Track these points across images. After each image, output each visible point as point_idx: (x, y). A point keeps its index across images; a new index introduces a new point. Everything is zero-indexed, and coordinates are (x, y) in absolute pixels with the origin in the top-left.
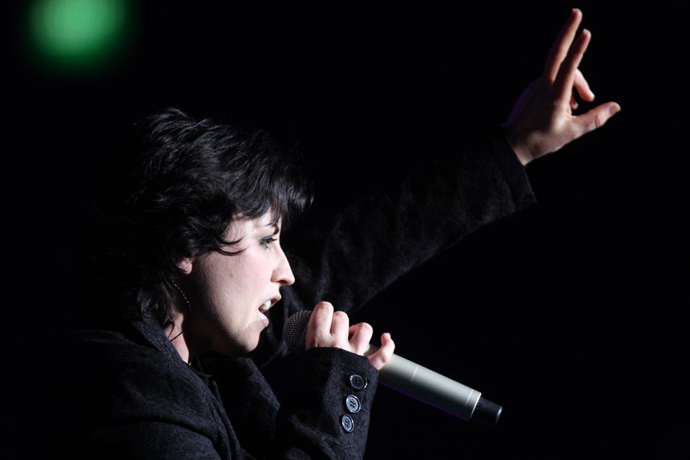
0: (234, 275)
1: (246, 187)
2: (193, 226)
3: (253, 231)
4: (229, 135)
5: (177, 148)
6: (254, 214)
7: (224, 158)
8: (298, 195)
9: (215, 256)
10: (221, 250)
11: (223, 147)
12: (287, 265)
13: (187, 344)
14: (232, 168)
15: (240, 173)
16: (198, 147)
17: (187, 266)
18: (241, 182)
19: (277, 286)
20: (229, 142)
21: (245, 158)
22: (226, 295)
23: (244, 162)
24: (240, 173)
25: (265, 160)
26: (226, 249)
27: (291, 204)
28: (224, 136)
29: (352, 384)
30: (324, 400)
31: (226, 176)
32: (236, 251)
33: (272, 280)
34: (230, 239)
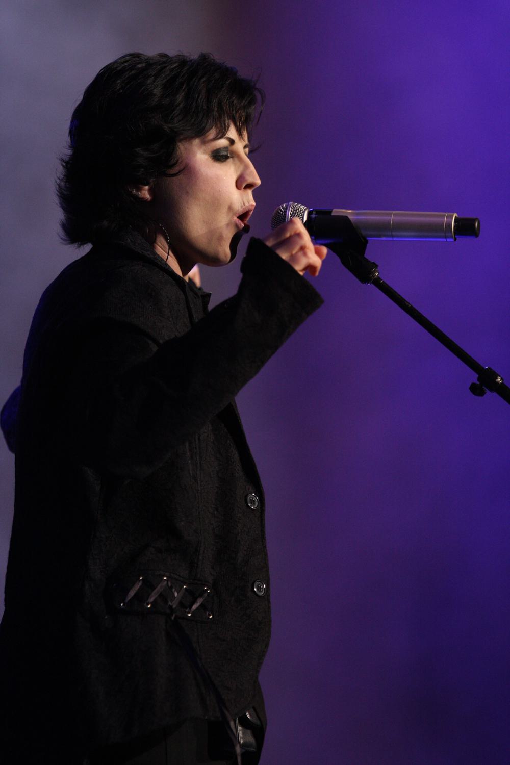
2: (362, 238)
6: (200, 133)
12: (252, 168)
17: (145, 193)
19: (250, 192)
22: (187, 210)
33: (238, 185)
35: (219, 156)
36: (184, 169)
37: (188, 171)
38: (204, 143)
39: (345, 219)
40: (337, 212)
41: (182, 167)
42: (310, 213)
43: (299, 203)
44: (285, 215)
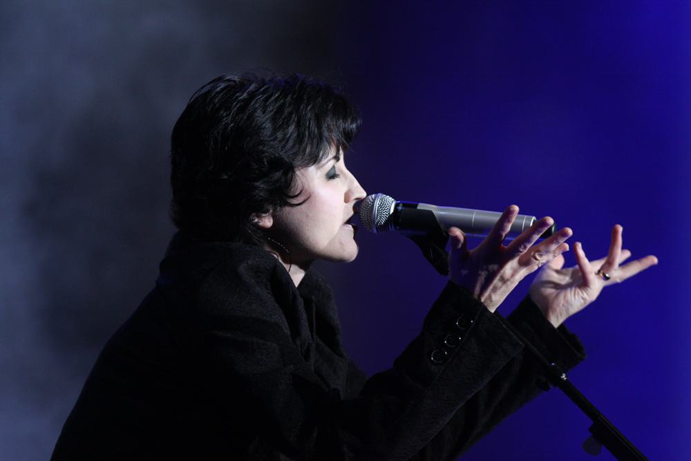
0: (310, 215)
1: (300, 139)
3: (317, 173)
4: (276, 93)
5: (232, 122)
6: (315, 159)
7: (274, 119)
8: (349, 121)
9: (287, 209)
10: (289, 203)
11: (271, 108)
12: (356, 183)
13: (363, 188)
14: (287, 123)
15: (292, 128)
16: (251, 116)
18: (295, 135)
20: (276, 100)
21: (290, 114)
23: (291, 118)
24: (292, 128)
25: (309, 108)
26: (295, 201)
27: (347, 135)
28: (271, 96)
29: (449, 346)
30: (578, 290)
31: (280, 135)
32: (300, 202)
33: (346, 200)
34: (291, 194)
35: (332, 176)
36: (299, 194)
37: (308, 197)
38: (318, 168)
39: (430, 213)
40: (422, 206)
41: (269, 94)
42: (397, 205)
43: (387, 195)
44: (373, 205)
